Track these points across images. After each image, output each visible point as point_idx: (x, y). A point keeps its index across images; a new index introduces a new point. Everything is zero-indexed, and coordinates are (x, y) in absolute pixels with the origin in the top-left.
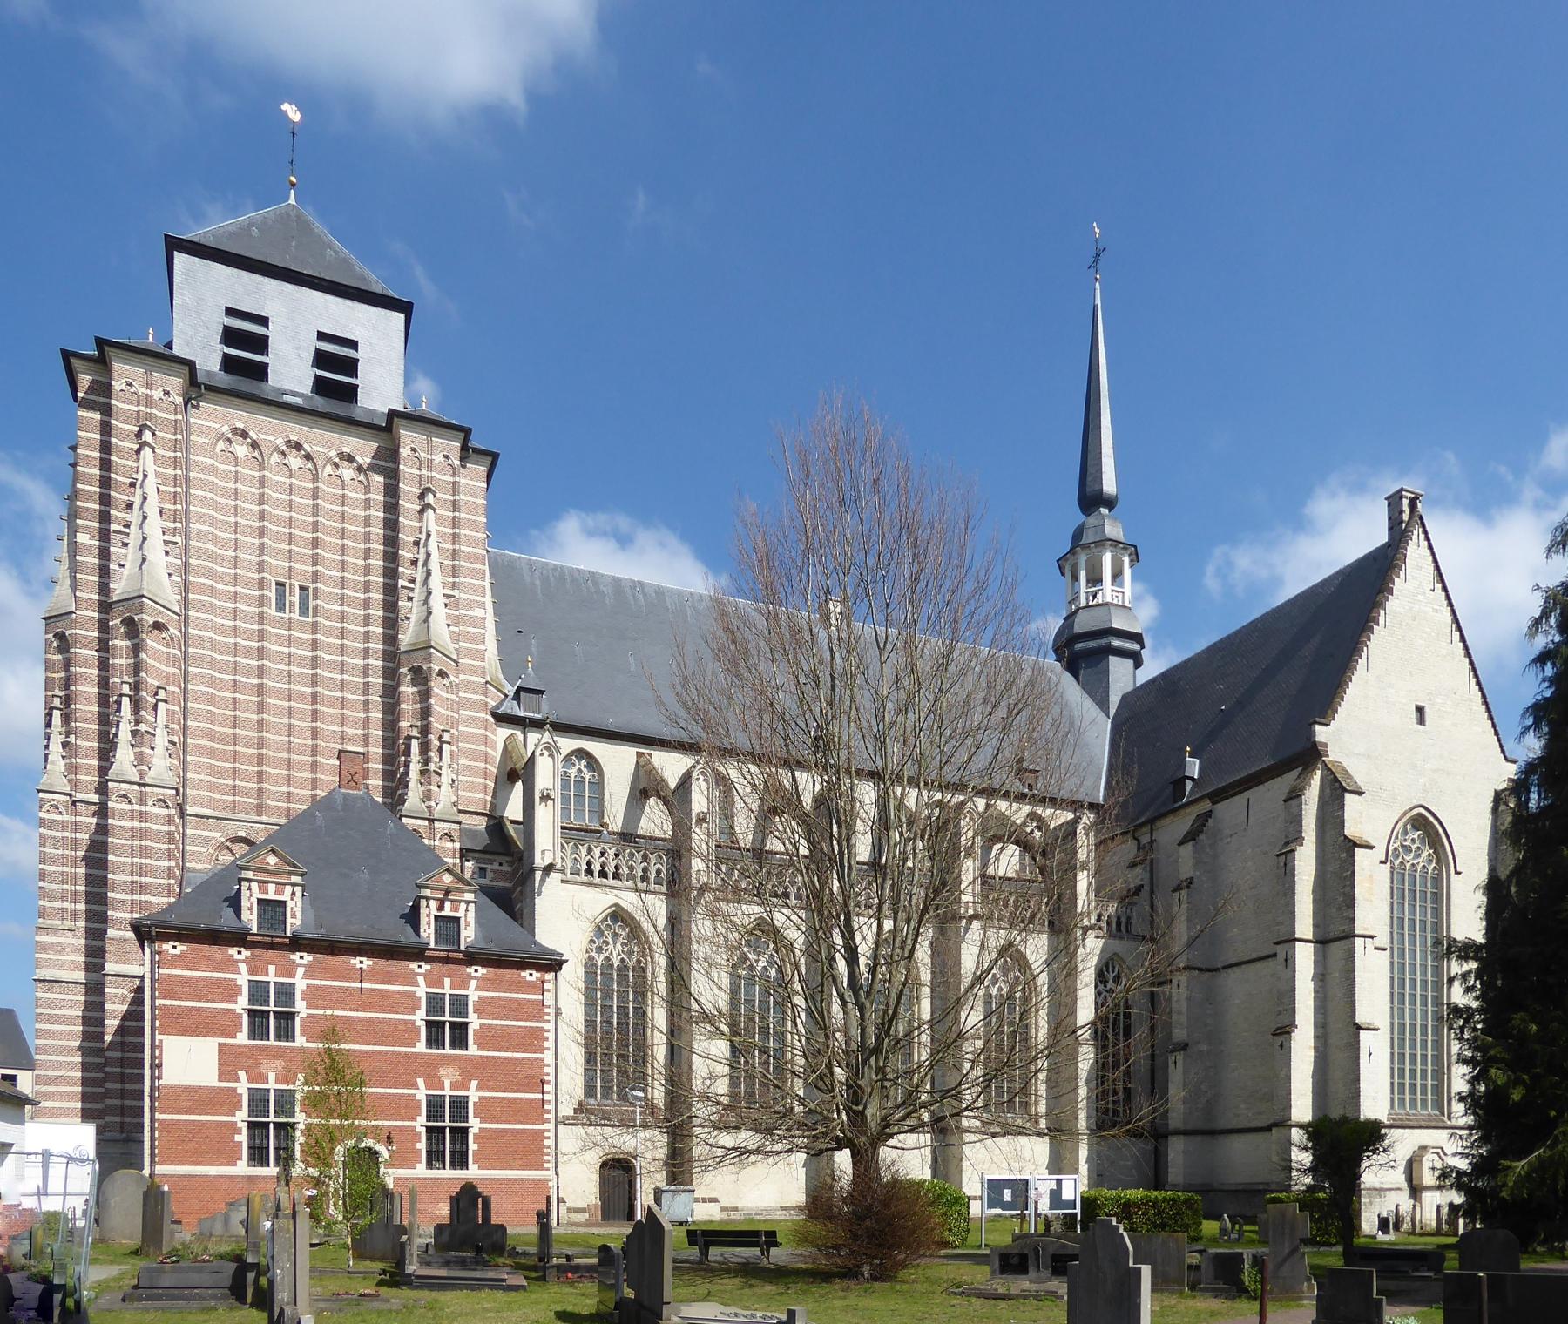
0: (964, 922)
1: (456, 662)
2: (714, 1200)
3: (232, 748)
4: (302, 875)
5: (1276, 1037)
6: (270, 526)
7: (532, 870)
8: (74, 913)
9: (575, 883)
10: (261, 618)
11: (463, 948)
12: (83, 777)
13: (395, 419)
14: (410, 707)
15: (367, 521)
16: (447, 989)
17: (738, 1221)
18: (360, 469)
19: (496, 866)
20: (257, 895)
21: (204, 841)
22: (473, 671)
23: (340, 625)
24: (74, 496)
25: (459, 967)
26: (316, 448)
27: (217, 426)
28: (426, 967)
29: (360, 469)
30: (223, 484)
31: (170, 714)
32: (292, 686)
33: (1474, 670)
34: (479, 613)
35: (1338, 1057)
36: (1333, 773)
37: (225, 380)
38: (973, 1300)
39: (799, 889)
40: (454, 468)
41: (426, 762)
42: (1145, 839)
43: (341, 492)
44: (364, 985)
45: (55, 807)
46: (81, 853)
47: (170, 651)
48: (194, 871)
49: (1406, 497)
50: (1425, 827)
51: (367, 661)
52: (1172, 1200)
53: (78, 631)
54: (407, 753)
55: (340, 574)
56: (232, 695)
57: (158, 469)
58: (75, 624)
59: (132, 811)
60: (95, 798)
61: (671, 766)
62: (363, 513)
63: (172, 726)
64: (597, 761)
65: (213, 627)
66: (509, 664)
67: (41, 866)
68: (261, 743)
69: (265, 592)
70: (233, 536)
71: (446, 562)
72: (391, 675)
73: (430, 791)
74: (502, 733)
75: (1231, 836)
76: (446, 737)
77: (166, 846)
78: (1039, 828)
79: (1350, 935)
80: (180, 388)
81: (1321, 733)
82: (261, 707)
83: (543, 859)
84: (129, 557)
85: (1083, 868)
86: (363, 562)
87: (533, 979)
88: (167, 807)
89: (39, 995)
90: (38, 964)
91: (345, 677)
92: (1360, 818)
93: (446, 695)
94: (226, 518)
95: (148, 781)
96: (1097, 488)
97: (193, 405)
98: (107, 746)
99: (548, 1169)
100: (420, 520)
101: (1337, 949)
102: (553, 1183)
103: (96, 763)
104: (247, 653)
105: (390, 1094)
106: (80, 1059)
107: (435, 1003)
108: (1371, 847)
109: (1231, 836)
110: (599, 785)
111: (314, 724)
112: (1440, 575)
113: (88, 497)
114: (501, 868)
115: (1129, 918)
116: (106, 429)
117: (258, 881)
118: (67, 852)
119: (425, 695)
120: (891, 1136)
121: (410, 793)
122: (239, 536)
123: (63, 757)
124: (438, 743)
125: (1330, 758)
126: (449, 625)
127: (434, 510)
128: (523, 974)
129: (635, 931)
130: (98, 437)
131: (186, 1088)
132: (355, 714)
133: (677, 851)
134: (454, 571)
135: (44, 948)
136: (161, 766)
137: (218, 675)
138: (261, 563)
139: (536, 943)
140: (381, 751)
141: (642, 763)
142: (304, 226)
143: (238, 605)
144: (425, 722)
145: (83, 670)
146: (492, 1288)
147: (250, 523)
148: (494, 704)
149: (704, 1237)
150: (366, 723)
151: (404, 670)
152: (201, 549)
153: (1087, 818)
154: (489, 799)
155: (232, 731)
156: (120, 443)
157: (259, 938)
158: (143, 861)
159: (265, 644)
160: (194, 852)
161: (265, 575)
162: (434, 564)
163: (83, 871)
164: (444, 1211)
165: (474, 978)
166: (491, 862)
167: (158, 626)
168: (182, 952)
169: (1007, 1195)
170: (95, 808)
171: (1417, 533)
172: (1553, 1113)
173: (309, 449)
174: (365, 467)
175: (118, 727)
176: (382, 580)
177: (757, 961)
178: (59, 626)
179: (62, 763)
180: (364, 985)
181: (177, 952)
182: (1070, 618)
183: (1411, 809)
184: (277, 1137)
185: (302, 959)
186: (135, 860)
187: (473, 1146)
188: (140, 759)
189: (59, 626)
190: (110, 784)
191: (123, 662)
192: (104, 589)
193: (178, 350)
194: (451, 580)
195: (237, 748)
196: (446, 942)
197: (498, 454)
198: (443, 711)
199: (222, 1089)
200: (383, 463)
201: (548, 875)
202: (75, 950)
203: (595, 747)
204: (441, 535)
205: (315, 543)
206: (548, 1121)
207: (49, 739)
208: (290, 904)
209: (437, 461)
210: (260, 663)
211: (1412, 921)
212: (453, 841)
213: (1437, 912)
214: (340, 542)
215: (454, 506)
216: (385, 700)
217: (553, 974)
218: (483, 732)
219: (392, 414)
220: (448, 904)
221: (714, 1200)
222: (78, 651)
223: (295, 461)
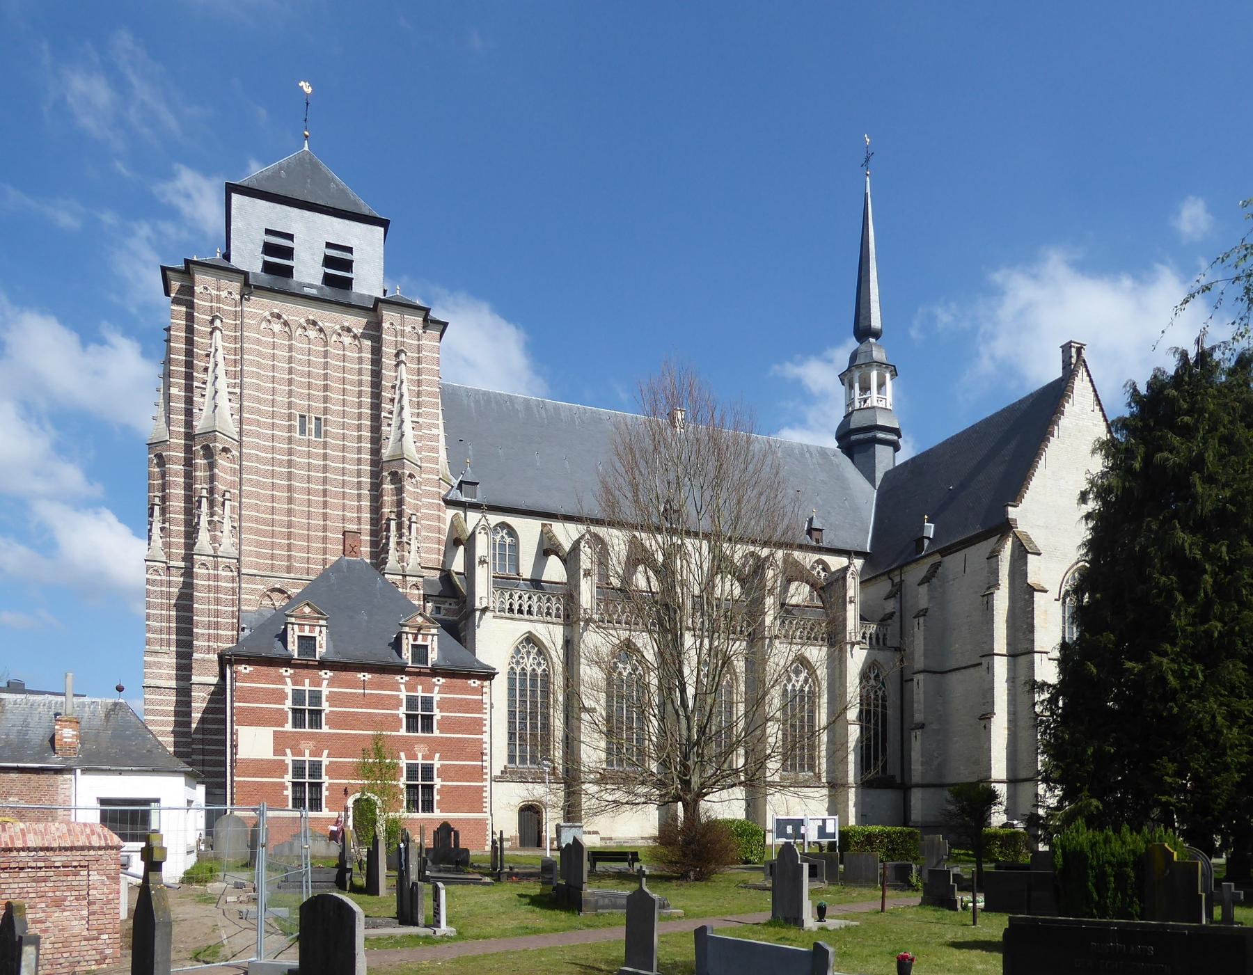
1: (420, 467)
2: (596, 833)
3: (270, 528)
4: (326, 619)
5: (982, 721)
6: (296, 378)
7: (474, 611)
8: (169, 641)
9: (502, 618)
10: (290, 440)
12: (174, 551)
13: (380, 304)
14: (389, 499)
15: (360, 372)
16: (420, 693)
17: (612, 846)
18: (355, 337)
19: (447, 606)
20: (297, 633)
21: (253, 591)
22: (431, 471)
23: (342, 443)
24: (168, 362)
26: (326, 324)
28: (406, 678)
29: (355, 337)
30: (264, 350)
31: (233, 507)
32: (310, 485)
34: (435, 431)
36: (1020, 540)
37: (266, 279)
38: (752, 890)
40: (418, 335)
41: (401, 536)
42: (897, 579)
43: (342, 353)
44: (366, 691)
46: (173, 602)
47: (232, 465)
48: (247, 611)
49: (1074, 347)
51: (360, 467)
52: (900, 833)
53: (171, 453)
54: (388, 529)
55: (342, 408)
56: (271, 493)
57: (224, 344)
58: (169, 448)
59: (209, 574)
60: (182, 564)
61: (566, 533)
62: (357, 367)
63: (234, 516)
64: (513, 529)
65: (259, 448)
66: (455, 464)
67: (147, 611)
68: (290, 525)
69: (293, 422)
70: (271, 385)
72: (376, 476)
73: (403, 555)
74: (450, 513)
75: (954, 580)
76: (414, 518)
77: (231, 597)
78: (824, 570)
79: (1031, 652)
80: (239, 290)
81: (1012, 512)
82: (290, 500)
83: (481, 603)
84: (206, 404)
85: (851, 602)
86: (357, 400)
87: (476, 685)
88: (232, 571)
89: (146, 696)
90: (145, 676)
91: (345, 478)
92: (1037, 571)
93: (413, 490)
94: (267, 373)
95: (220, 554)
96: (867, 324)
97: (246, 299)
98: (191, 530)
99: (486, 812)
100: (396, 371)
101: (1023, 660)
102: (489, 822)
103: (183, 541)
104: (281, 463)
106: (173, 739)
107: (411, 703)
108: (1046, 591)
109: (954, 580)
110: (515, 547)
112: (1098, 400)
113: (178, 362)
114: (451, 607)
115: (885, 635)
116: (190, 318)
117: (298, 624)
118: (164, 601)
119: (400, 491)
120: (706, 794)
121: (390, 557)
122: (275, 385)
123: (161, 537)
124: (408, 523)
125: (1019, 530)
127: (405, 364)
128: (469, 682)
129: (542, 651)
130: (184, 322)
131: (253, 760)
133: (570, 594)
134: (419, 405)
135: (149, 665)
136: (227, 543)
137: (261, 479)
138: (290, 403)
139: (477, 661)
140: (369, 527)
141: (545, 531)
142: (315, 166)
143: (275, 432)
144: (399, 509)
145: (175, 479)
146: (474, 883)
147: (282, 376)
148: (444, 493)
149: (598, 856)
150: (359, 509)
151: (385, 474)
152: (250, 395)
153: (858, 563)
154: (441, 558)
155: (271, 517)
156: (200, 328)
158: (216, 607)
159: (293, 457)
160: (246, 599)
161: (293, 411)
162: (405, 402)
163: (174, 613)
164: (429, 842)
165: (437, 685)
166: (444, 603)
167: (225, 450)
168: (250, 671)
169: (789, 829)
170: (182, 571)
171: (1082, 372)
172: (1078, 785)
173: (321, 325)
175: (199, 518)
177: (798, 681)
178: (158, 450)
179: (161, 541)
180: (366, 691)
181: (247, 671)
182: (848, 416)
184: (310, 792)
185: (326, 674)
186: (211, 607)
187: (436, 797)
188: (214, 539)
189: (158, 450)
190: (195, 556)
191: (202, 474)
192: (189, 424)
193: (236, 261)
194: (417, 411)
195: (274, 528)
196: (419, 662)
197: (447, 323)
198: (411, 501)
199: (275, 760)
200: (371, 332)
201: (484, 614)
203: (513, 521)
204: (410, 381)
205: (326, 388)
206: (486, 780)
207: (151, 525)
208: (318, 639)
209: (223, 297)
210: (289, 470)
212: (418, 589)
214: (342, 386)
215: (419, 361)
217: (489, 682)
218: (437, 513)
219: (378, 301)
220: (420, 637)
221: (596, 833)
222: (171, 466)
223: (312, 333)
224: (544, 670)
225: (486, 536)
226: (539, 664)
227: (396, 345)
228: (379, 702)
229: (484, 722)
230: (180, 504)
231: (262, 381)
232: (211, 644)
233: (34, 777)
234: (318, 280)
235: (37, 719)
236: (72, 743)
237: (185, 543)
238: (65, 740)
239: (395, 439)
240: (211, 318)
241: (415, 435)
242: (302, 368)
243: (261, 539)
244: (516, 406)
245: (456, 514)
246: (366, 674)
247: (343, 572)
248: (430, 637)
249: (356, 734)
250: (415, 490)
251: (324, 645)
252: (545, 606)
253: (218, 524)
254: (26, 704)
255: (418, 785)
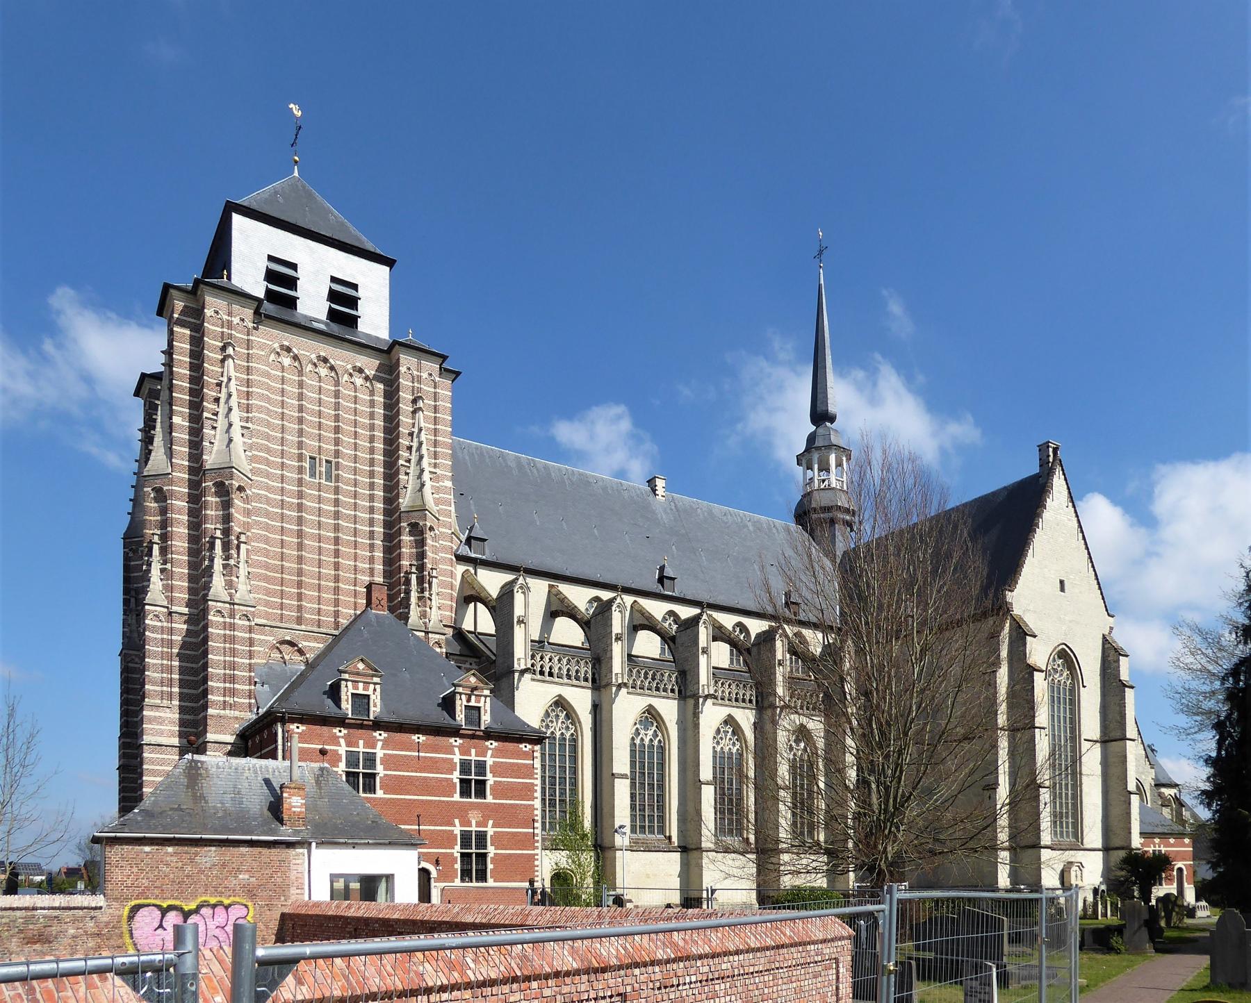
0: (614, 689)
1: (438, 520)
5: (986, 792)
11: (483, 728)
12: (177, 595)
14: (408, 551)
16: (361, 748)
18: (367, 378)
20: (351, 691)
25: (481, 741)
26: (338, 362)
27: (271, 343)
28: (460, 741)
29: (367, 378)
33: (1090, 558)
35: (1116, 811)
36: (1018, 623)
39: (673, 685)
43: (353, 394)
44: (421, 754)
45: (156, 616)
46: (176, 651)
47: (246, 506)
50: (1066, 657)
53: (174, 488)
58: (171, 483)
60: (186, 610)
71: (431, 449)
74: (460, 569)
84: (217, 437)
86: (369, 445)
87: (527, 749)
92: (1039, 653)
94: (276, 409)
100: (413, 418)
105: (437, 830)
111: (336, 560)
113: (181, 390)
117: (352, 681)
119: (421, 543)
123: (161, 579)
125: (1015, 613)
126: (433, 493)
127: (233, 359)
129: (571, 714)
132: (363, 553)
145: (177, 516)
151: (404, 524)
152: (259, 431)
154: (453, 615)
156: (210, 354)
157: (353, 721)
163: (177, 663)
165: (490, 749)
166: (465, 662)
170: (186, 617)
174: (371, 377)
176: (382, 458)
177: (646, 735)
179: (161, 583)
180: (421, 754)
183: (1059, 646)
185: (381, 736)
187: (490, 866)
188: (230, 585)
191: (213, 513)
196: (360, 713)
202: (171, 722)
208: (373, 697)
209: (235, 323)
211: (1059, 717)
212: (441, 647)
213: (1072, 712)
216: (386, 544)
220: (473, 698)
223: (323, 371)
224: (572, 735)
225: (523, 595)
226: (567, 728)
227: (413, 390)
228: (434, 765)
229: (535, 788)
230: (183, 544)
231: (270, 416)
232: (227, 699)
233: (265, 851)
234: (323, 315)
235: (246, 785)
236: (301, 812)
237: (189, 587)
238: (293, 809)
239: (414, 488)
240: (221, 344)
241: (432, 486)
242: (313, 407)
243: (270, 586)
244: (509, 463)
245: (467, 570)
246: (420, 736)
247: (373, 626)
248: (483, 698)
249: (410, 800)
250: (434, 544)
251: (378, 704)
252: (574, 669)
253: (234, 569)
254: (230, 768)
255: (472, 853)
